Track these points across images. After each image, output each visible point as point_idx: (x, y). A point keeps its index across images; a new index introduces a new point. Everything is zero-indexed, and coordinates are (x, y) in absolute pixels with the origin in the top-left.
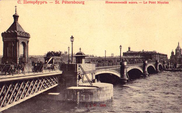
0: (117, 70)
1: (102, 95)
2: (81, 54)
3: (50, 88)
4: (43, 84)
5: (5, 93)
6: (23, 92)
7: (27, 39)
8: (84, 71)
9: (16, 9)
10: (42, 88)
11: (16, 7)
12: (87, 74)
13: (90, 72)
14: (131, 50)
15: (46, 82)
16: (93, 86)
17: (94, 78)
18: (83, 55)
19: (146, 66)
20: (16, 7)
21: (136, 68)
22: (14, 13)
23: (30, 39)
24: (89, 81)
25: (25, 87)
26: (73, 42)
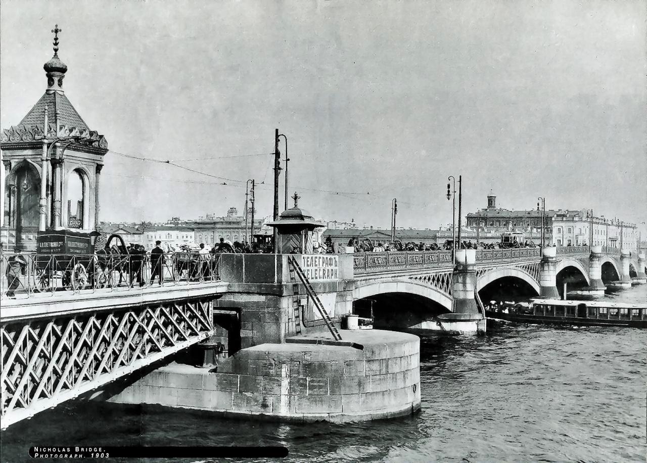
0: (438, 280)
1: (378, 377)
2: (302, 217)
3: (179, 346)
4: (153, 331)
5: (26, 360)
6: (110, 351)
7: (97, 157)
8: (310, 281)
9: (56, 39)
10: (148, 348)
11: (56, 31)
12: (319, 296)
13: (331, 288)
14: (498, 205)
15: (190, 317)
16: (344, 341)
17: (349, 308)
18: (307, 221)
19: (442, 315)
20: (56, 31)
21: (514, 273)
22: (48, 57)
23: (108, 154)
24: (327, 322)
25: (59, 349)
26: (58, 52)
